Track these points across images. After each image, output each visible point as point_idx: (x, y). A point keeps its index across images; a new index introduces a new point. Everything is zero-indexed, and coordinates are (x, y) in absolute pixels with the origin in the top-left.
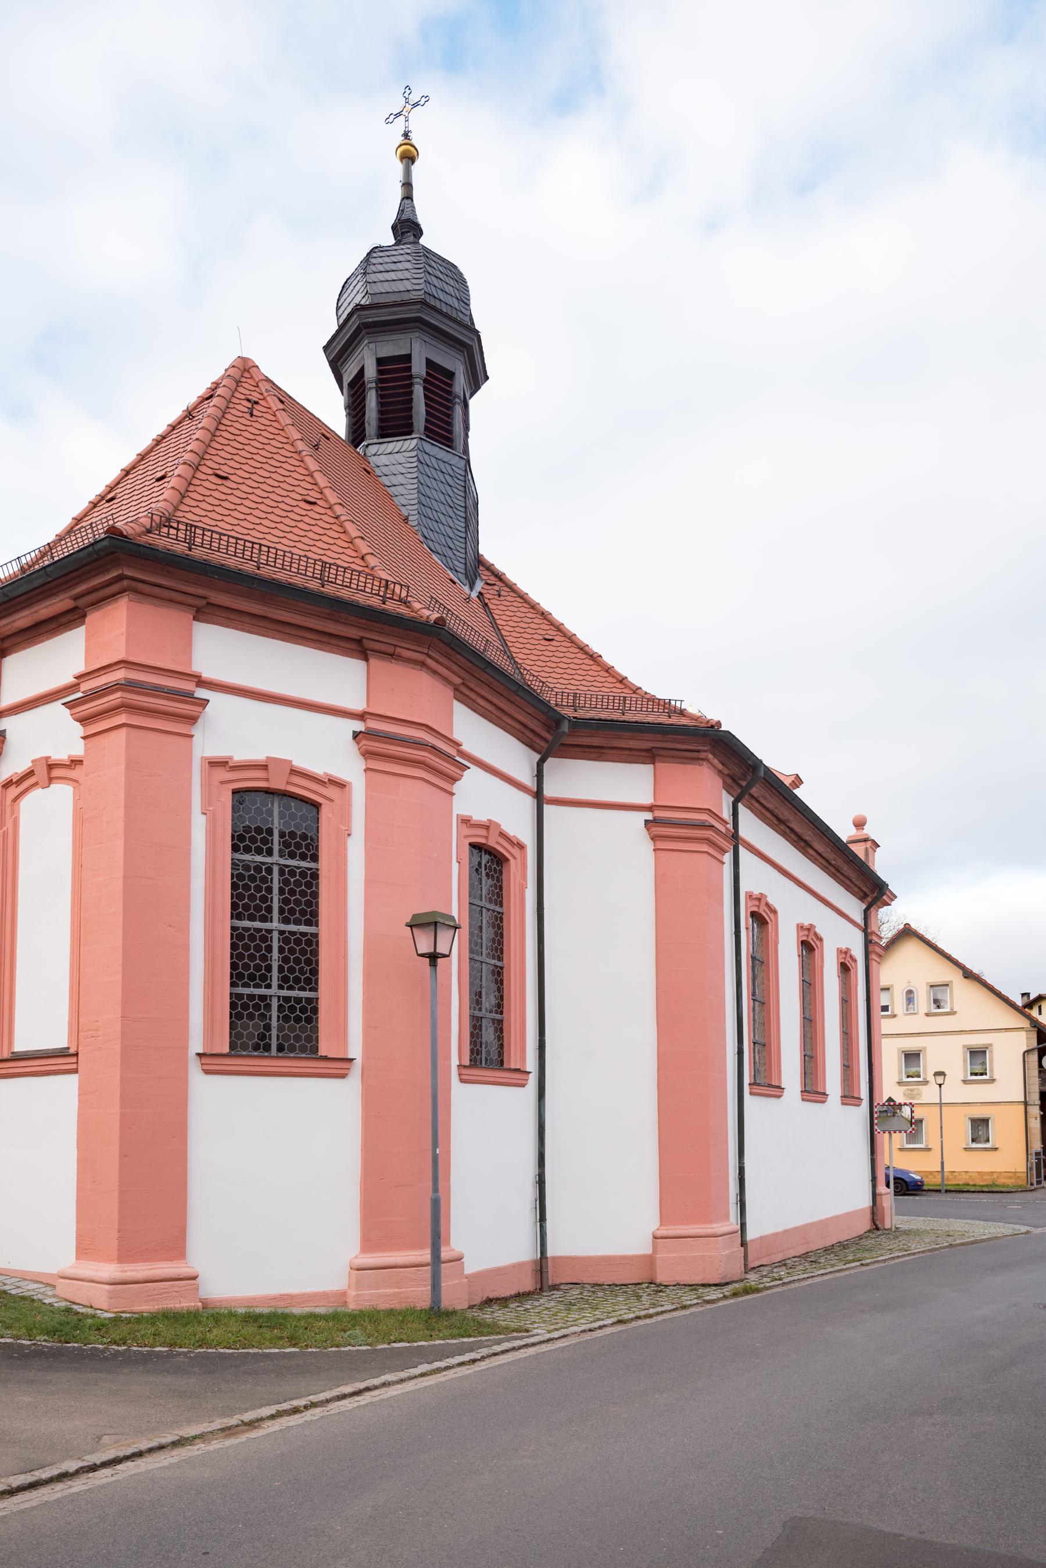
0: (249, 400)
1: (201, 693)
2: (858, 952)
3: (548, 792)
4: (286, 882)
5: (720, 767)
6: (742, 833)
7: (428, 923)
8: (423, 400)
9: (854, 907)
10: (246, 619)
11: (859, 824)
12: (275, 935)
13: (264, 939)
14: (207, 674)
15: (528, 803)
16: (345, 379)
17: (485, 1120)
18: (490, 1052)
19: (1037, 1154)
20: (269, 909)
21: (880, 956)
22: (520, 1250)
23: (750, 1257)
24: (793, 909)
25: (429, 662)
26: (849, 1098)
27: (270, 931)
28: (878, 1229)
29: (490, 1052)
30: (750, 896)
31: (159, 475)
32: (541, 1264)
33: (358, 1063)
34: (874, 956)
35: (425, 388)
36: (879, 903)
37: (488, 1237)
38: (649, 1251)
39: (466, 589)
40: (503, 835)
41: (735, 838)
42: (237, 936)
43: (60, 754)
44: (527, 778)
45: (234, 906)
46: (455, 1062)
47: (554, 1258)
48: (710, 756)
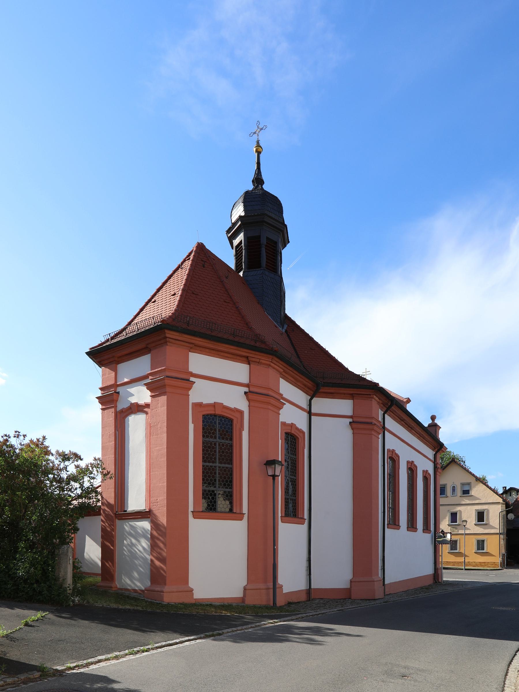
0: (202, 261)
1: (192, 379)
2: (431, 471)
3: (313, 411)
4: (221, 448)
5: (378, 400)
6: (386, 426)
7: (271, 463)
8: (264, 252)
9: (430, 453)
10: (207, 350)
11: (433, 418)
12: (217, 468)
13: (213, 469)
14: (195, 371)
15: (305, 415)
16: (234, 244)
17: (290, 536)
18: (293, 510)
19: (504, 555)
20: (215, 459)
21: (440, 473)
22: (301, 585)
23: (386, 590)
24: (405, 456)
25: (272, 364)
26: (426, 529)
27: (215, 467)
28: (436, 582)
29: (293, 510)
30: (389, 450)
31: (172, 293)
32: (309, 591)
33: (246, 517)
34: (438, 473)
35: (266, 249)
36: (440, 451)
37: (291, 579)
38: (349, 587)
39: (281, 329)
40: (297, 429)
41: (384, 427)
42: (204, 468)
43: (141, 402)
44: (305, 406)
45: (203, 458)
46: (280, 515)
47: (314, 589)
48: (375, 397)
